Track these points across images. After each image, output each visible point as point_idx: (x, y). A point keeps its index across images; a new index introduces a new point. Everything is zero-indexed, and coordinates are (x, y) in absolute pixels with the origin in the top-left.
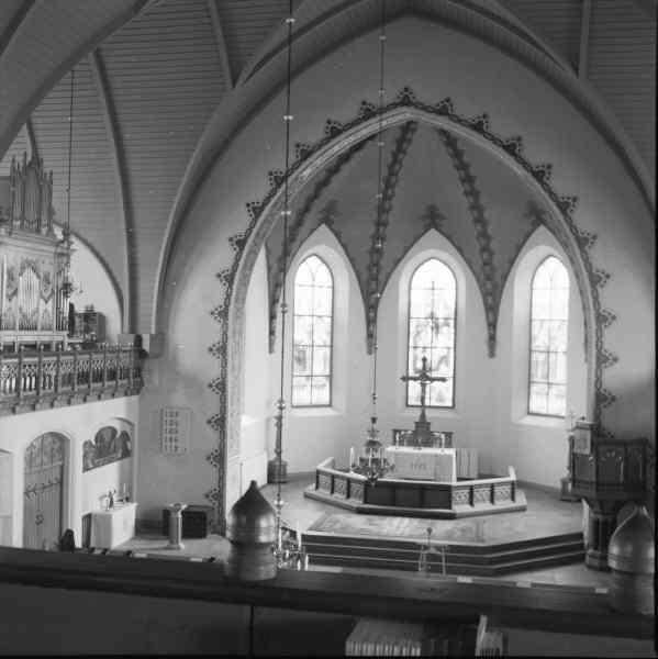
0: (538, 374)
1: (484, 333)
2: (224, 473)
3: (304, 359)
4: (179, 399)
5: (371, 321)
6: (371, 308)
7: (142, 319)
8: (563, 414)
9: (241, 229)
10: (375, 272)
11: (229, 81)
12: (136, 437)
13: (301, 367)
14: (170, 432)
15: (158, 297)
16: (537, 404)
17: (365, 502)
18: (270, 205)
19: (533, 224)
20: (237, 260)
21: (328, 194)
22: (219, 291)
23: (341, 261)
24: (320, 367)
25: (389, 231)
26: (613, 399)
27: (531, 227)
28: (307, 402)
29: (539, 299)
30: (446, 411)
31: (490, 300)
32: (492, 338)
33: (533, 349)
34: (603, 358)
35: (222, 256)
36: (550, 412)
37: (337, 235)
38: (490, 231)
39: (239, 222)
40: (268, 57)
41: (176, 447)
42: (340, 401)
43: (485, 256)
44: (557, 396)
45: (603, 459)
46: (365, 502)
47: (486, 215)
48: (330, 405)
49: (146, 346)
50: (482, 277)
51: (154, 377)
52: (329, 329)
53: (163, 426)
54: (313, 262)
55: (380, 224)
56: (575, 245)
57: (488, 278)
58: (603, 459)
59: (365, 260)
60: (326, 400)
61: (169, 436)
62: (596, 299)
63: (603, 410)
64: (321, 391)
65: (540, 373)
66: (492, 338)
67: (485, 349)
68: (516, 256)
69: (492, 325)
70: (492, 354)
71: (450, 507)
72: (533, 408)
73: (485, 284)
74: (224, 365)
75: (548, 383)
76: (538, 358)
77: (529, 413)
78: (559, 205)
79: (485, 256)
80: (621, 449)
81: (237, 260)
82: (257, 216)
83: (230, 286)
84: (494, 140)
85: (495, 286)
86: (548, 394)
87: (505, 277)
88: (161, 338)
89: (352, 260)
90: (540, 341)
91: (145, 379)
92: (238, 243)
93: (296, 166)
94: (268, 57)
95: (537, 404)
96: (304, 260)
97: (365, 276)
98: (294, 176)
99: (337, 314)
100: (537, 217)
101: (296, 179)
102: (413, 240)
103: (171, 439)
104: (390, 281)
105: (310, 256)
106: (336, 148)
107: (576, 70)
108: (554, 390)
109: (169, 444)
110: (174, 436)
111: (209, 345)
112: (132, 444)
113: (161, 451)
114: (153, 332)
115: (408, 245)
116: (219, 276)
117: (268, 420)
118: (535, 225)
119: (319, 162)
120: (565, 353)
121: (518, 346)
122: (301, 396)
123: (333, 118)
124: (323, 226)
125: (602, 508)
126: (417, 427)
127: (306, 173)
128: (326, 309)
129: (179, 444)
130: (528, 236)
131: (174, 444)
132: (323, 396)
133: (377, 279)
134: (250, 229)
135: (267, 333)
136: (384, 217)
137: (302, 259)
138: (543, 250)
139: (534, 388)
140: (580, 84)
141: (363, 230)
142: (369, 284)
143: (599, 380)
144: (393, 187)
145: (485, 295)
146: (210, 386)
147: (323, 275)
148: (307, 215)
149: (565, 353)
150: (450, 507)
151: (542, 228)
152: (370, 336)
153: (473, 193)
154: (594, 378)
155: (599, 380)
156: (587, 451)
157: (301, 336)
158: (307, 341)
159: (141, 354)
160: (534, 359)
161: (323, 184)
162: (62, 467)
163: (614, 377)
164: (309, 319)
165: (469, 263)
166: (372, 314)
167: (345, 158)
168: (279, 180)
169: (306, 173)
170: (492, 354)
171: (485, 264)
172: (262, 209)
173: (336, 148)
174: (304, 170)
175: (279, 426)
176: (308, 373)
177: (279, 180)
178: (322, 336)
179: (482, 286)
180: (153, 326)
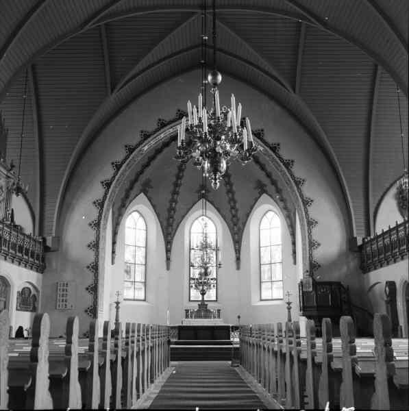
0: (265, 277)
1: (233, 255)
3: (130, 271)
4: (68, 276)
5: (168, 251)
6: (168, 243)
7: (46, 229)
8: (282, 297)
9: (109, 176)
11: (110, 91)
12: (40, 299)
13: (128, 277)
14: (63, 296)
15: (59, 208)
16: (265, 295)
18: (107, 200)
19: (259, 193)
20: (106, 194)
21: (143, 178)
22: (95, 213)
23: (153, 217)
24: (139, 277)
25: (179, 198)
26: (319, 266)
27: (259, 195)
28: (132, 297)
30: (213, 303)
31: (236, 237)
32: (238, 259)
33: (262, 263)
35: (97, 192)
36: (274, 298)
37: (150, 200)
39: (108, 172)
40: (134, 77)
41: (66, 305)
43: (233, 212)
44: (277, 288)
45: (319, 293)
46: (179, 339)
47: (234, 188)
48: (145, 300)
49: (49, 243)
50: (232, 225)
51: (54, 261)
52: (144, 254)
53: (57, 295)
54: (136, 215)
55: (175, 193)
56: (294, 184)
58: (319, 293)
59: (166, 214)
60: (143, 298)
61: (61, 293)
62: (306, 213)
63: (314, 273)
66: (238, 259)
67: (234, 266)
68: (250, 212)
69: (238, 251)
70: (238, 268)
72: (263, 298)
73: (233, 229)
74: (97, 256)
76: (265, 268)
77: (261, 300)
79: (233, 212)
81: (106, 194)
83: (108, 189)
85: (239, 229)
87: (244, 224)
88: (58, 239)
89: (158, 215)
90: (266, 259)
91: (47, 265)
93: (140, 143)
94: (134, 77)
95: (265, 295)
96: (130, 214)
97: (165, 224)
98: (139, 149)
100: (262, 189)
101: (140, 150)
102: (186, 211)
103: (63, 295)
104: (179, 229)
105: (134, 211)
106: (162, 136)
107: (294, 91)
108: (275, 285)
109: (61, 303)
110: (64, 298)
111: (88, 242)
112: (38, 304)
113: (56, 309)
114: (54, 235)
115: (189, 207)
116: (95, 203)
117: (111, 305)
118: (260, 194)
119: (152, 142)
122: (129, 294)
124: (142, 194)
126: (200, 308)
129: (67, 303)
130: (256, 200)
131: (64, 303)
132: (141, 295)
133: (172, 226)
134: (114, 177)
135: (111, 252)
136: (177, 189)
137: (130, 212)
138: (266, 207)
139: (264, 286)
140: (295, 99)
141: (164, 197)
142: (167, 229)
143: (311, 255)
144: (183, 170)
145: (233, 234)
146: (88, 267)
148: (141, 176)
152: (168, 259)
154: (308, 255)
155: (311, 255)
156: (311, 289)
157: (128, 256)
158: (132, 261)
159: (47, 249)
161: (152, 158)
162: (5, 303)
163: (319, 254)
164: (133, 248)
165: (224, 217)
168: (131, 150)
170: (238, 268)
171: (234, 216)
172: (121, 166)
173: (162, 136)
174: (145, 146)
175: (117, 308)
177: (108, 185)
178: (140, 259)
179: (231, 229)
180: (54, 231)
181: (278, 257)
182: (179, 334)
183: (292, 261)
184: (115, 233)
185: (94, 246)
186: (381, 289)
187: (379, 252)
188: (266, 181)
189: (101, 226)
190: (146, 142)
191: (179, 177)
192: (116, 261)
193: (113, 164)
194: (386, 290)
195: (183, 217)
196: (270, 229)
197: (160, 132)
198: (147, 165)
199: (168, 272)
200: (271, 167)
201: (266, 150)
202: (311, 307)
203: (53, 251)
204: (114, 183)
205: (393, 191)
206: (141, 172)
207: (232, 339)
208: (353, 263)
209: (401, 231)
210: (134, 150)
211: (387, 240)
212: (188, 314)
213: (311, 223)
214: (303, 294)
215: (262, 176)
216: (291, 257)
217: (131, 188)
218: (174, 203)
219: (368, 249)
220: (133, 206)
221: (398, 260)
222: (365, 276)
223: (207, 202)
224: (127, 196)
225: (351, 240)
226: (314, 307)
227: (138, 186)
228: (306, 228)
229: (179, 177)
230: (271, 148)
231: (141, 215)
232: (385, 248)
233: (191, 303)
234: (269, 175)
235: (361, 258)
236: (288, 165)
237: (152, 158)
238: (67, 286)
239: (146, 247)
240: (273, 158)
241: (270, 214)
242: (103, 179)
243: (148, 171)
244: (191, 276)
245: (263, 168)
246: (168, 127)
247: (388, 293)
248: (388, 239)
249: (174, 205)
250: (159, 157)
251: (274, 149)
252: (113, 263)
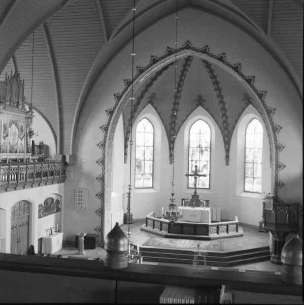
0: (249, 173)
1: (224, 154)
2: (103, 219)
3: (141, 166)
4: (83, 185)
5: (171, 149)
6: (172, 142)
7: (65, 148)
8: (260, 192)
9: (111, 106)
10: (173, 126)
11: (106, 37)
12: (63, 202)
13: (139, 170)
14: (79, 200)
15: (73, 138)
16: (248, 187)
17: (169, 232)
19: (246, 104)
20: (110, 120)
21: (151, 90)
22: (101, 134)
23: (158, 121)
24: (148, 170)
25: (180, 107)
26: (283, 185)
27: (245, 105)
28: (142, 186)
29: (249, 139)
30: (206, 190)
31: (226, 139)
32: (227, 157)
33: (246, 161)
34: (279, 166)
35: (102, 118)
36: (254, 191)
37: (156, 109)
38: (226, 107)
39: (111, 103)
40: (124, 26)
41: (81, 207)
42: (157, 185)
43: (224, 118)
44: (258, 183)
45: (279, 212)
46: (169, 232)
47: (225, 99)
48: (152, 188)
49: (68, 160)
50: (223, 128)
51: (71, 175)
52: (152, 152)
53: (75, 197)
54: (145, 121)
55: (175, 104)
56: (266, 113)
57: (226, 129)
58: (279, 212)
59: (169, 120)
60: (151, 185)
61: (78, 202)
62: (275, 138)
63: (279, 190)
65: (249, 173)
66: (227, 157)
67: (224, 161)
68: (239, 119)
69: (227, 151)
70: (227, 164)
71: (208, 235)
72: (246, 189)
73: (224, 132)
74: (104, 169)
75: (253, 177)
76: (249, 165)
77: (244, 191)
78: (258, 95)
79: (224, 118)
80: (287, 208)
81: (110, 120)
82: (119, 100)
84: (228, 65)
85: (229, 132)
86: (253, 182)
87: (233, 128)
88: (74, 156)
89: (163, 120)
90: (249, 158)
92: (110, 112)
93: (137, 77)
94: (124, 26)
95: (248, 187)
96: (141, 120)
97: (169, 128)
98: (136, 81)
99: (156, 145)
100: (248, 100)
101: (137, 83)
102: (191, 111)
103: (79, 203)
104: (180, 130)
105: (143, 119)
106: (155, 69)
107: (266, 32)
108: (256, 181)
109: (78, 205)
110: (80, 202)
111: (97, 160)
112: (61, 206)
113: (74, 209)
114: (71, 154)
115: (188, 113)
116: (101, 128)
117: (124, 194)
118: (247, 104)
119: (147, 75)
120: (261, 163)
121: (239, 160)
122: (139, 183)
123: (154, 55)
124: (149, 104)
125: (278, 235)
126: (193, 198)
127: (141, 80)
128: (150, 143)
129: (83, 206)
130: (244, 109)
131: (80, 205)
132: (149, 183)
133: (174, 129)
134: (116, 106)
135: (124, 154)
136: (177, 101)
137: (139, 120)
138: (251, 116)
139: (247, 180)
140: (268, 39)
141: (168, 106)
142: (170, 131)
143: (277, 176)
144: (181, 86)
145: (224, 137)
146: (97, 179)
147: (149, 127)
148: (142, 99)
149: (261, 163)
150: (208, 235)
151: (250, 106)
152: (171, 155)
153: (218, 89)
154: (274, 175)
155: (277, 176)
156: (271, 209)
157: (139, 155)
158: (142, 158)
159: (65, 164)
160: (246, 166)
161: (149, 85)
162: (29, 216)
163: (283, 175)
164: (143, 148)
165: (217, 122)
166: (172, 146)
167: (159, 73)
168: (129, 83)
169: (141, 80)
170: (227, 164)
171: (224, 122)
172: (121, 97)
173: (155, 69)
174: (140, 79)
175: (129, 197)
176: (142, 172)
177: (129, 83)
178: (149, 156)
179: (223, 132)
180: (71, 151)
238: (82, 197)
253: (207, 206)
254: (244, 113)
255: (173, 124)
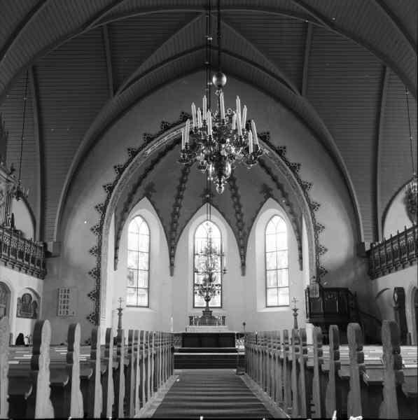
0: (271, 283)
1: (238, 261)
3: (133, 277)
4: (69, 282)
5: (172, 256)
6: (172, 248)
7: (47, 235)
8: (288, 304)
9: (111, 180)
11: (112, 93)
12: (41, 305)
13: (131, 283)
14: (64, 303)
15: (60, 212)
16: (271, 301)
19: (265, 197)
20: (108, 198)
21: (146, 182)
22: (97, 217)
23: (156, 222)
24: (142, 283)
25: (183, 203)
26: (326, 272)
27: (264, 200)
28: (135, 304)
30: (218, 309)
31: (242, 242)
32: (243, 265)
33: (267, 269)
35: (99, 196)
36: (280, 304)
37: (153, 204)
39: (111, 176)
40: (137, 79)
41: (67, 312)
43: (238, 216)
44: (283, 294)
45: (326, 299)
46: (183, 347)
47: (239, 192)
48: (148, 307)
49: (50, 249)
50: (237, 230)
51: (55, 267)
52: (147, 260)
53: (58, 302)
54: (139, 219)
55: (179, 197)
56: (300, 188)
58: (326, 299)
59: (169, 219)
60: (146, 304)
61: (63, 300)
62: (313, 217)
63: (321, 279)
64: (143, 299)
66: (243, 265)
67: (239, 271)
68: (256, 216)
69: (243, 257)
70: (243, 274)
72: (269, 304)
73: (239, 234)
74: (99, 261)
76: (271, 274)
77: (267, 307)
79: (238, 216)
81: (108, 198)
85: (244, 234)
87: (250, 229)
88: (60, 244)
89: (162, 220)
90: (271, 265)
93: (143, 147)
94: (137, 79)
95: (271, 301)
96: (133, 218)
97: (169, 229)
98: (142, 152)
100: (267, 193)
101: (143, 154)
102: (190, 216)
103: (64, 301)
104: (183, 234)
105: (137, 216)
106: (166, 138)
107: (301, 93)
108: (281, 291)
109: (62, 310)
110: (66, 305)
111: (90, 248)
112: (39, 311)
113: (57, 315)
114: (55, 240)
115: (193, 211)
116: (97, 207)
117: (113, 312)
118: (266, 199)
119: (156, 146)
122: (131, 300)
124: (145, 198)
126: (204, 314)
129: (69, 310)
130: (262, 204)
131: (66, 310)
132: (144, 301)
133: (175, 231)
134: (117, 181)
135: (113, 257)
136: (181, 193)
137: (132, 216)
138: (272, 211)
139: (269, 292)
140: (302, 101)
141: (168, 201)
142: (171, 234)
143: (318, 261)
144: (187, 174)
145: (238, 239)
146: (90, 273)
148: (144, 180)
152: (172, 265)
154: (315, 261)
155: (318, 261)
156: (318, 296)
157: (131, 262)
158: (135, 267)
159: (48, 254)
161: (155, 162)
162: (5, 309)
163: (326, 260)
164: (136, 254)
165: (229, 222)
168: (134, 153)
170: (243, 274)
171: (239, 221)
172: (123, 169)
173: (166, 138)
174: (148, 149)
175: (120, 315)
177: (110, 189)
178: (143, 264)
179: (236, 234)
180: (55, 236)
181: (284, 262)
182: (183, 341)
183: (299, 266)
184: (117, 239)
185: (96, 251)
186: (389, 295)
187: (388, 257)
188: (272, 185)
189: (104, 231)
190: (149, 145)
191: (183, 181)
192: (118, 266)
193: (115, 167)
194: (394, 296)
195: (187, 222)
196: (276, 234)
197: (163, 135)
198: (151, 168)
199: (172, 278)
200: (277, 171)
201: (272, 154)
202: (318, 314)
203: (54, 257)
204: (116, 187)
205: (402, 195)
206: (145, 176)
207: (237, 347)
208: (361, 269)
209: (410, 236)
210: (137, 153)
211: (396, 246)
212: (192, 320)
213: (318, 228)
214: (309, 300)
215: (267, 180)
216: (298, 263)
217: (134, 192)
218: (178, 208)
219: (376, 254)
220: (136, 211)
221: (406, 265)
222: (373, 282)
223: (212, 207)
224: (130, 201)
225: (359, 245)
226: (321, 314)
227: (141, 190)
228: (313, 233)
229: (183, 181)
230: (277, 151)
231: (144, 220)
232: (393, 253)
233: (195, 309)
234: (275, 179)
235: (369, 263)
236: (294, 168)
237: (155, 162)
239: (149, 253)
240: (279, 161)
241: (276, 219)
242: (105, 182)
243: (152, 174)
244: (196, 282)
245: (269, 171)
246: (172, 130)
247: (396, 299)
248: (397, 244)
249: (177, 210)
250: (163, 160)
251: (280, 152)
252: (115, 269)
253: (224, 324)
254: (261, 210)
255: (175, 224)
